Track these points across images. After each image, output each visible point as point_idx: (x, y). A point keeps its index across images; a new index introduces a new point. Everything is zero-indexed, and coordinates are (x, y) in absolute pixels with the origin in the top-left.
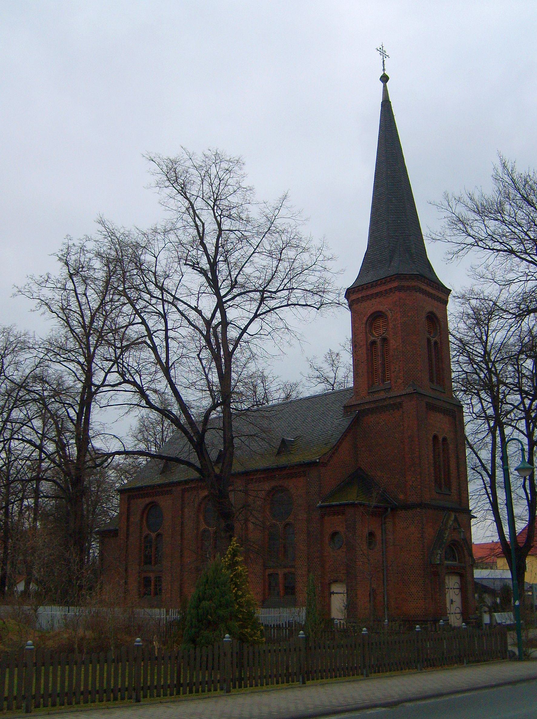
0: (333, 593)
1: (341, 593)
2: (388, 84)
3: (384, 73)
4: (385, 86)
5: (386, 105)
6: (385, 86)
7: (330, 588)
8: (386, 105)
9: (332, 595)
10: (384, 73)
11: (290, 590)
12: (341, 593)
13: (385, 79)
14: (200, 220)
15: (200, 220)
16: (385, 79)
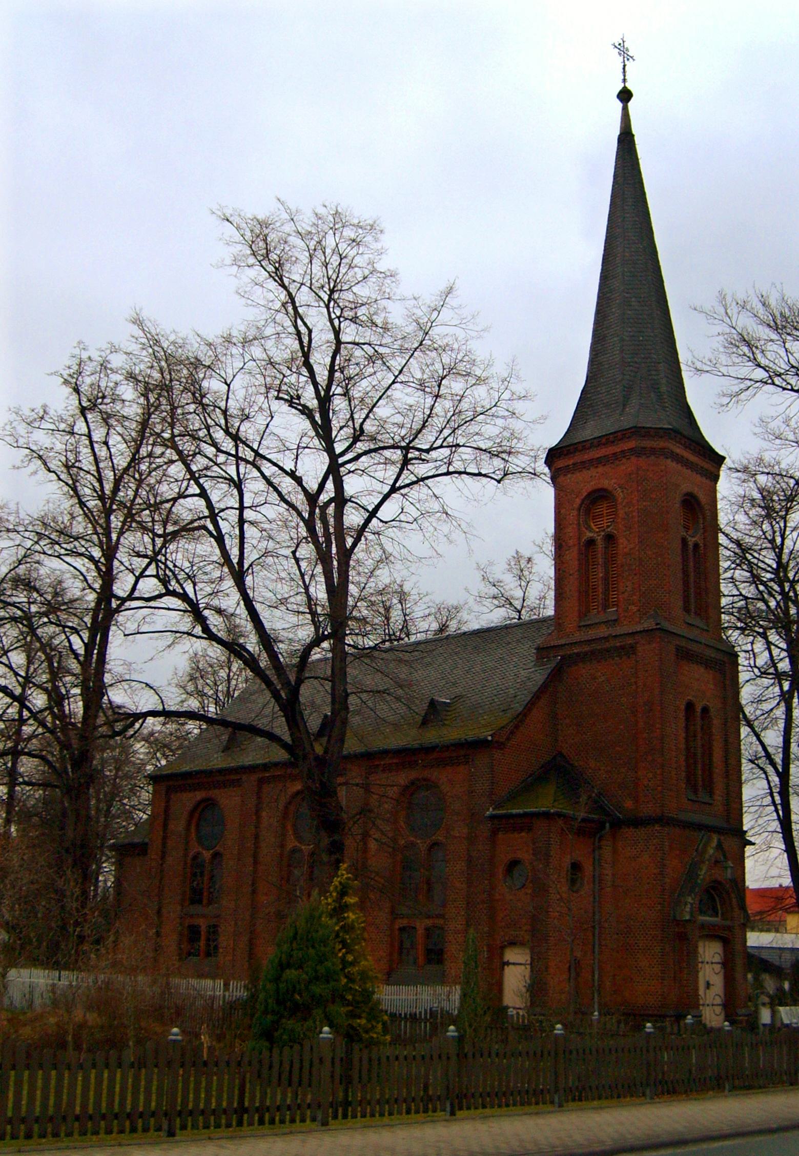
0: (508, 963)
1: (521, 964)
2: (630, 104)
3: (625, 87)
4: (625, 111)
5: (626, 140)
6: (625, 111)
7: (501, 955)
8: (626, 140)
9: (506, 967)
10: (625, 87)
11: (436, 956)
12: (521, 964)
13: (625, 96)
14: (305, 324)
15: (305, 324)
16: (625, 96)
